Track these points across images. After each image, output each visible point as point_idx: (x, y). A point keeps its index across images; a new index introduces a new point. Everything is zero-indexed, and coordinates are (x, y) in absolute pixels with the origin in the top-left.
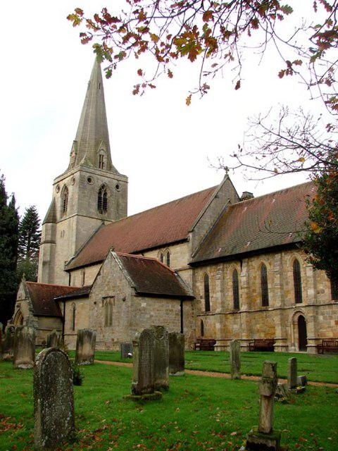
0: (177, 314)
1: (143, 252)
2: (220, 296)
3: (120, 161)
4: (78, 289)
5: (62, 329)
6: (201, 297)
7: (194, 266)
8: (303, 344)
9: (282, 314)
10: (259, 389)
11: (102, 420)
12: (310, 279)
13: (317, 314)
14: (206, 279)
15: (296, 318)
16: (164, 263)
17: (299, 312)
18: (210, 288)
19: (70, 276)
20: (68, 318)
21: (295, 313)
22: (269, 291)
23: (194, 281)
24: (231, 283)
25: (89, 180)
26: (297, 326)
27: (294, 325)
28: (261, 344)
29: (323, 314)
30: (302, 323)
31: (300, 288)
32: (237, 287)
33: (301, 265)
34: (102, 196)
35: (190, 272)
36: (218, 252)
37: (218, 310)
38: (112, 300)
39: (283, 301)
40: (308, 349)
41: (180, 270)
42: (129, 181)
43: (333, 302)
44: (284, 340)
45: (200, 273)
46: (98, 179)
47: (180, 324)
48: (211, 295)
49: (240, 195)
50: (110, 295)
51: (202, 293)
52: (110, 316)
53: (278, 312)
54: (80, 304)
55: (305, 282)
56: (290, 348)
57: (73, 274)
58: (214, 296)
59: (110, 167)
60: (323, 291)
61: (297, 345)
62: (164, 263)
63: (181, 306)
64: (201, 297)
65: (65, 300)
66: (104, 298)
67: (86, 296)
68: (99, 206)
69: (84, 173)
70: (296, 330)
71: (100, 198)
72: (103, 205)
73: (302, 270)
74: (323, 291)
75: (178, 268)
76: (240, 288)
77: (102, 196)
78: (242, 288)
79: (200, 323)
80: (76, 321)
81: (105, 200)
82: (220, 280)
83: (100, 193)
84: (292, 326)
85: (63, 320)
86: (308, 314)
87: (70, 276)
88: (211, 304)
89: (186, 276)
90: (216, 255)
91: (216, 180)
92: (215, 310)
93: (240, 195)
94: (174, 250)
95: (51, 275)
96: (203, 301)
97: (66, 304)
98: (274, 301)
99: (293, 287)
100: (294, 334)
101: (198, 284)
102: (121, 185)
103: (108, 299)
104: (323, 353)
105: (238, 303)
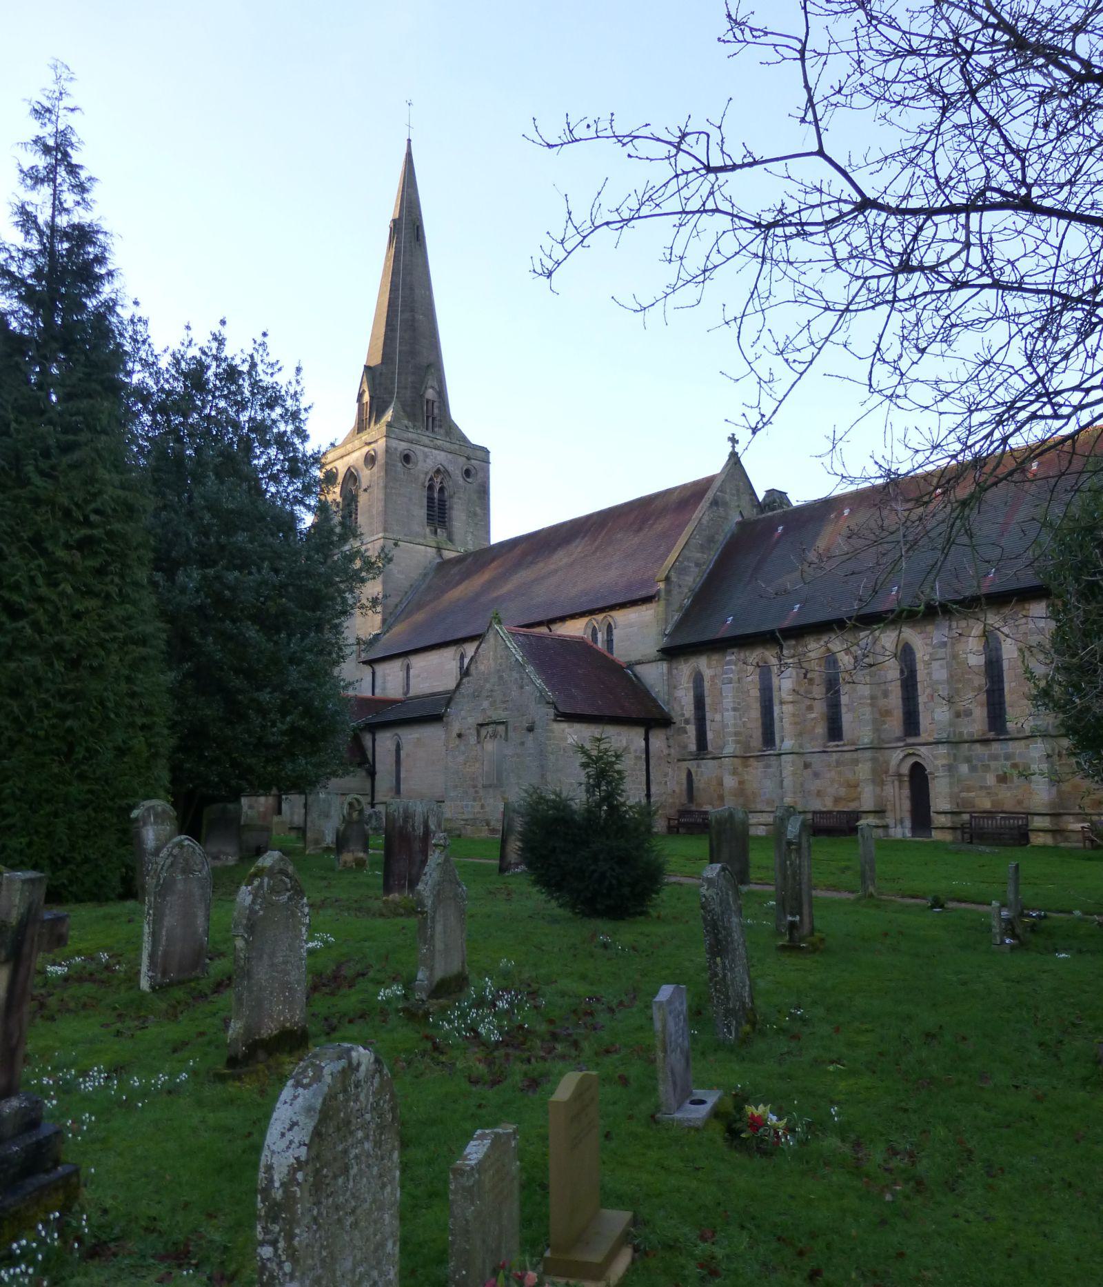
0: (637, 758)
1: (549, 622)
2: (731, 716)
3: (470, 411)
4: (393, 702)
5: (369, 791)
6: (687, 722)
7: (671, 653)
8: (921, 816)
9: (874, 760)
10: (68, 530)
11: (742, 1132)
12: (940, 687)
13: (955, 760)
14: (698, 680)
15: (905, 769)
16: (600, 645)
17: (913, 754)
18: (708, 700)
19: (374, 673)
20: (384, 764)
21: (906, 756)
22: (844, 709)
23: (672, 686)
24: (755, 693)
25: (407, 458)
26: (907, 785)
27: (901, 782)
28: (824, 822)
29: (968, 760)
30: (918, 778)
31: (916, 705)
32: (770, 700)
33: (919, 655)
34: (436, 495)
35: (664, 666)
36: (728, 625)
37: (730, 749)
38: (501, 728)
39: (877, 730)
40: (934, 833)
41: (639, 663)
42: (492, 458)
43: (991, 735)
44: (880, 812)
45: (685, 669)
46: (426, 456)
47: (644, 778)
48: (708, 716)
49: (761, 496)
50: (495, 718)
51: (689, 711)
52: (471, 758)
53: (868, 754)
54: (410, 736)
55: (928, 691)
56: (892, 831)
57: (380, 669)
58: (718, 717)
59: (452, 431)
60: (968, 713)
61: (908, 823)
62: (600, 645)
63: (647, 740)
64: (687, 722)
65: (373, 728)
66: (481, 725)
67: (436, 719)
68: (430, 518)
69: (394, 443)
70: (906, 792)
71: (430, 499)
72: (438, 513)
73: (920, 667)
74: (968, 713)
75: (634, 657)
76: (776, 701)
77: (436, 495)
78: (781, 703)
79: (684, 776)
80: (402, 775)
81: (442, 503)
82: (730, 683)
83: (431, 488)
84: (896, 783)
85: (372, 774)
86: (935, 759)
87: (374, 673)
88: (710, 735)
89: (653, 675)
90: (722, 632)
91: (712, 465)
92: (722, 748)
93: (761, 496)
94: (621, 618)
95: (770, 897)
96: (692, 729)
97: (378, 736)
98: (857, 725)
99: (900, 702)
100: (899, 798)
101: (680, 693)
102: (475, 464)
103: (490, 729)
104: (971, 843)
105: (772, 733)
